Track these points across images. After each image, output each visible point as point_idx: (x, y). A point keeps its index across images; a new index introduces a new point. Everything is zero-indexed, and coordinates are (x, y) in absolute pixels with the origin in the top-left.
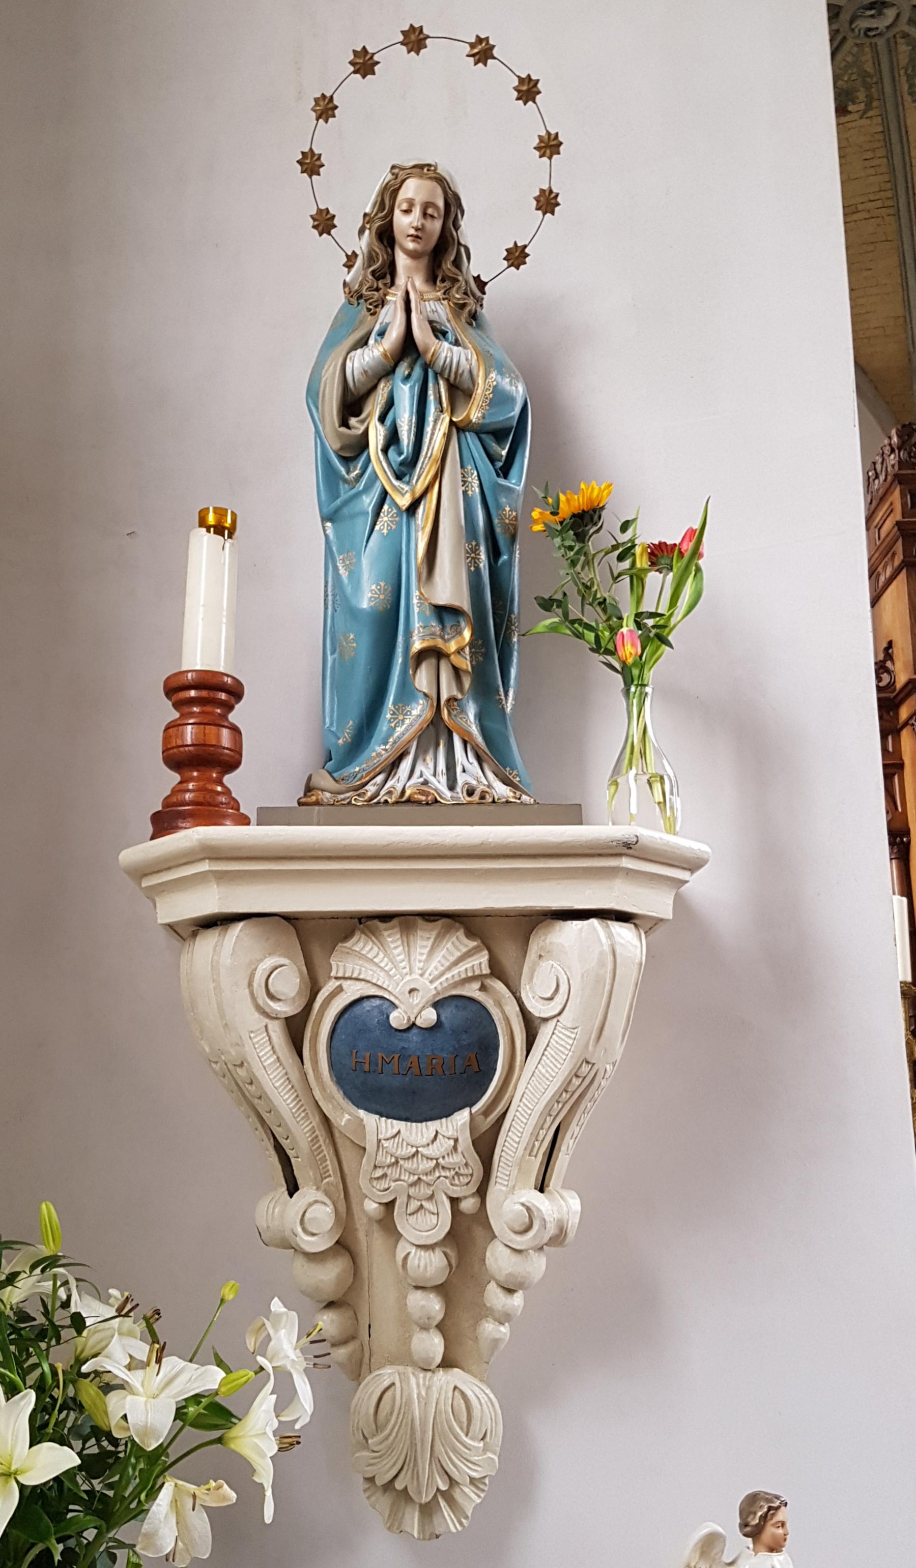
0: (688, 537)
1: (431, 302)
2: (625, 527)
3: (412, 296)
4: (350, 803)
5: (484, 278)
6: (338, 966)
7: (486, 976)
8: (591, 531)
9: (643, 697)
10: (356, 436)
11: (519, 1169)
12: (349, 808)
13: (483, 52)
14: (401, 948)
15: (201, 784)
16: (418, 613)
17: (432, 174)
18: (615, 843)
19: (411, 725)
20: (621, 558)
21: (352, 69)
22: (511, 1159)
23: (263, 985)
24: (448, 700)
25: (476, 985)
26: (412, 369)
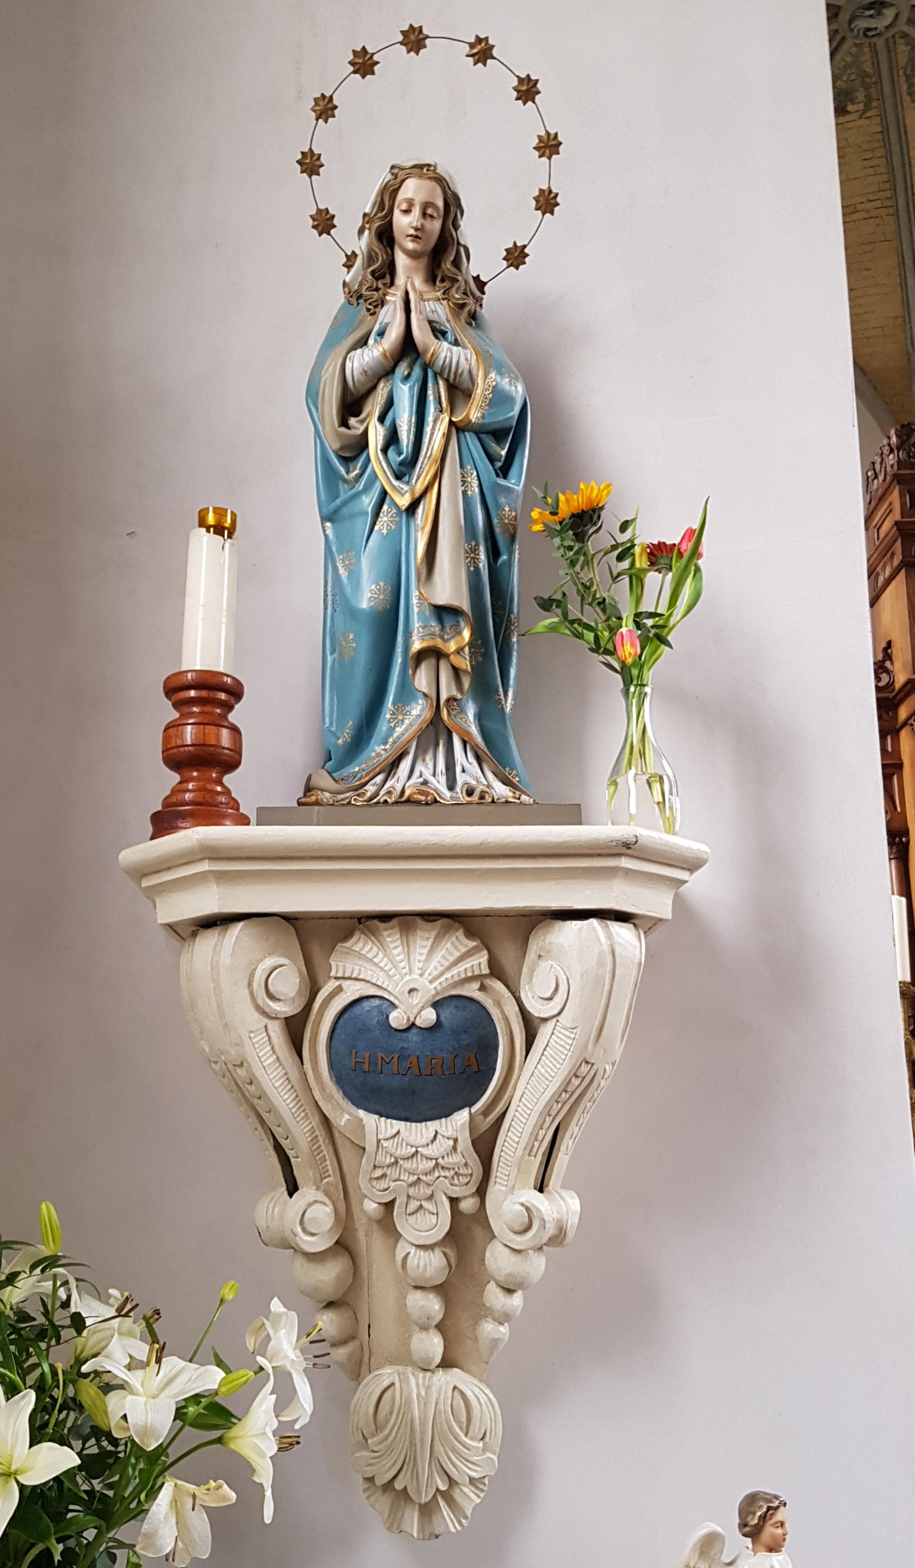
0: (687, 537)
1: (431, 302)
2: (624, 527)
3: (412, 296)
4: (349, 803)
5: (483, 278)
6: (337, 966)
7: (485, 976)
8: (591, 531)
9: (642, 697)
10: (356, 436)
11: (519, 1169)
12: (348, 808)
13: (482, 52)
14: (401, 948)
15: (201, 784)
16: (418, 613)
17: (431, 174)
18: (614, 843)
19: (411, 725)
20: (620, 558)
21: (351, 69)
22: (510, 1159)
23: (263, 985)
24: (448, 700)
25: (476, 985)
26: (412, 369)
